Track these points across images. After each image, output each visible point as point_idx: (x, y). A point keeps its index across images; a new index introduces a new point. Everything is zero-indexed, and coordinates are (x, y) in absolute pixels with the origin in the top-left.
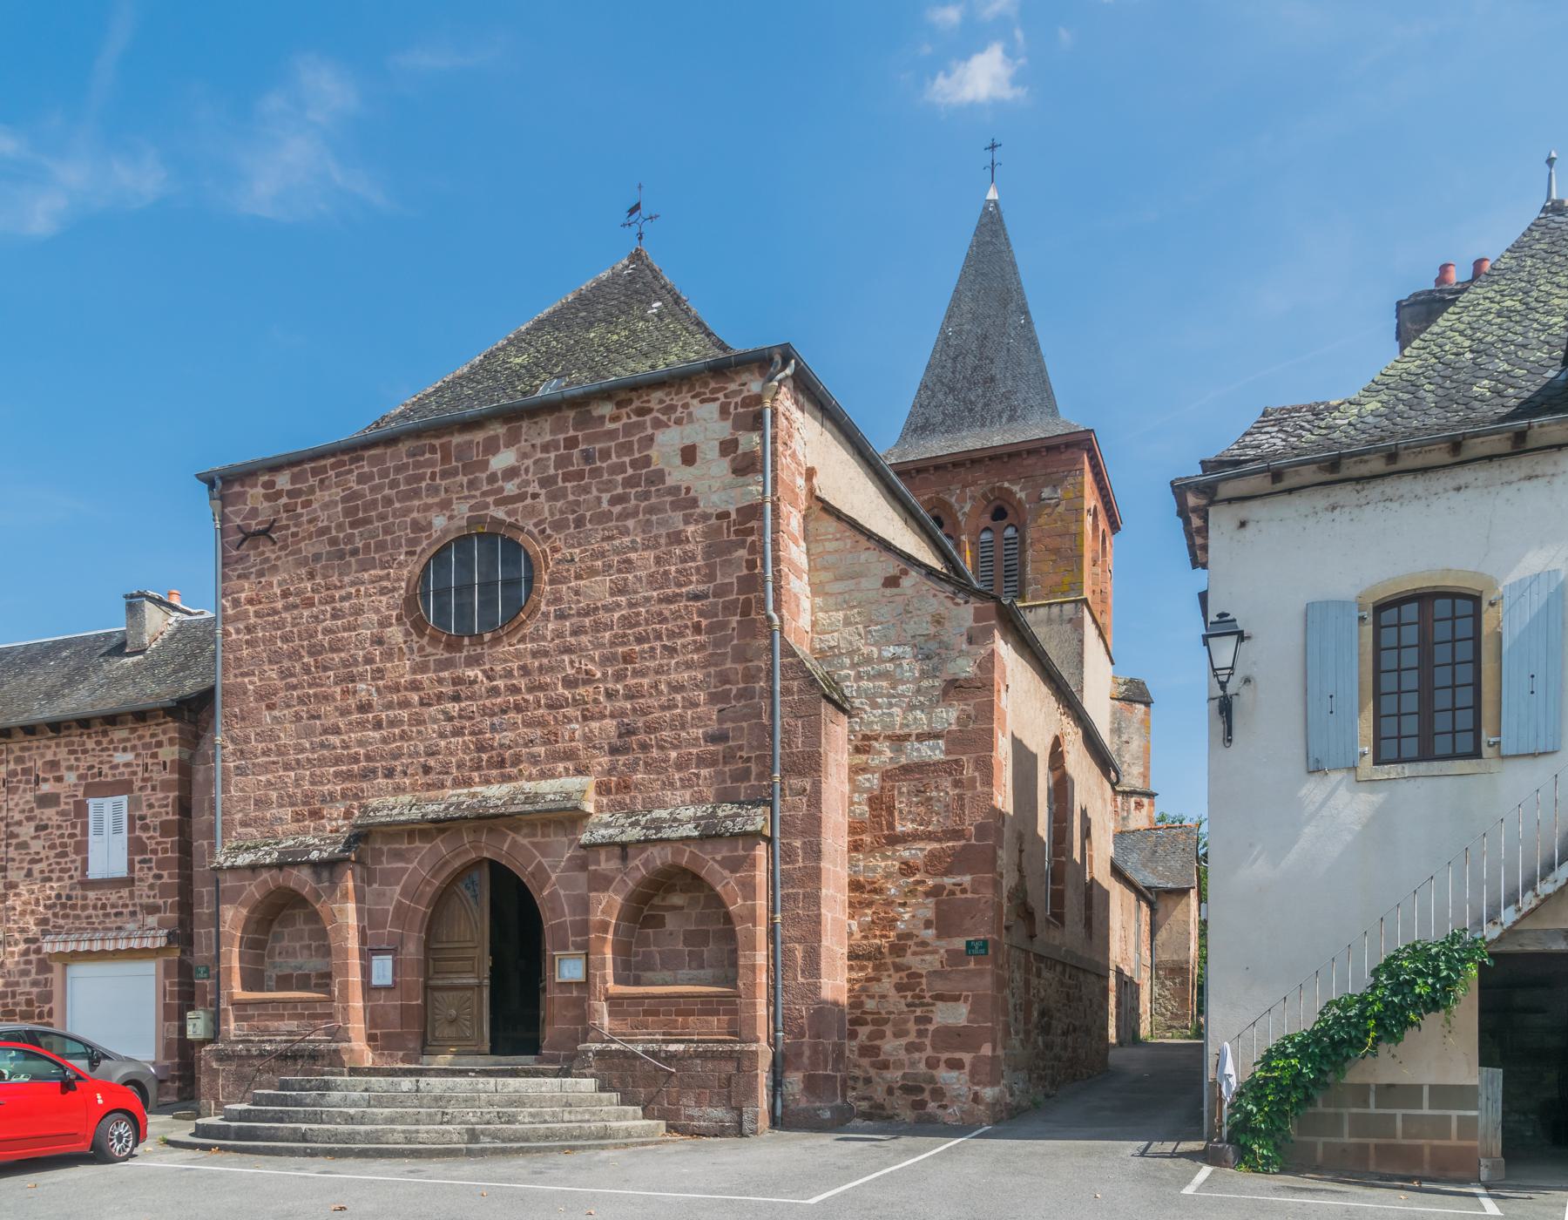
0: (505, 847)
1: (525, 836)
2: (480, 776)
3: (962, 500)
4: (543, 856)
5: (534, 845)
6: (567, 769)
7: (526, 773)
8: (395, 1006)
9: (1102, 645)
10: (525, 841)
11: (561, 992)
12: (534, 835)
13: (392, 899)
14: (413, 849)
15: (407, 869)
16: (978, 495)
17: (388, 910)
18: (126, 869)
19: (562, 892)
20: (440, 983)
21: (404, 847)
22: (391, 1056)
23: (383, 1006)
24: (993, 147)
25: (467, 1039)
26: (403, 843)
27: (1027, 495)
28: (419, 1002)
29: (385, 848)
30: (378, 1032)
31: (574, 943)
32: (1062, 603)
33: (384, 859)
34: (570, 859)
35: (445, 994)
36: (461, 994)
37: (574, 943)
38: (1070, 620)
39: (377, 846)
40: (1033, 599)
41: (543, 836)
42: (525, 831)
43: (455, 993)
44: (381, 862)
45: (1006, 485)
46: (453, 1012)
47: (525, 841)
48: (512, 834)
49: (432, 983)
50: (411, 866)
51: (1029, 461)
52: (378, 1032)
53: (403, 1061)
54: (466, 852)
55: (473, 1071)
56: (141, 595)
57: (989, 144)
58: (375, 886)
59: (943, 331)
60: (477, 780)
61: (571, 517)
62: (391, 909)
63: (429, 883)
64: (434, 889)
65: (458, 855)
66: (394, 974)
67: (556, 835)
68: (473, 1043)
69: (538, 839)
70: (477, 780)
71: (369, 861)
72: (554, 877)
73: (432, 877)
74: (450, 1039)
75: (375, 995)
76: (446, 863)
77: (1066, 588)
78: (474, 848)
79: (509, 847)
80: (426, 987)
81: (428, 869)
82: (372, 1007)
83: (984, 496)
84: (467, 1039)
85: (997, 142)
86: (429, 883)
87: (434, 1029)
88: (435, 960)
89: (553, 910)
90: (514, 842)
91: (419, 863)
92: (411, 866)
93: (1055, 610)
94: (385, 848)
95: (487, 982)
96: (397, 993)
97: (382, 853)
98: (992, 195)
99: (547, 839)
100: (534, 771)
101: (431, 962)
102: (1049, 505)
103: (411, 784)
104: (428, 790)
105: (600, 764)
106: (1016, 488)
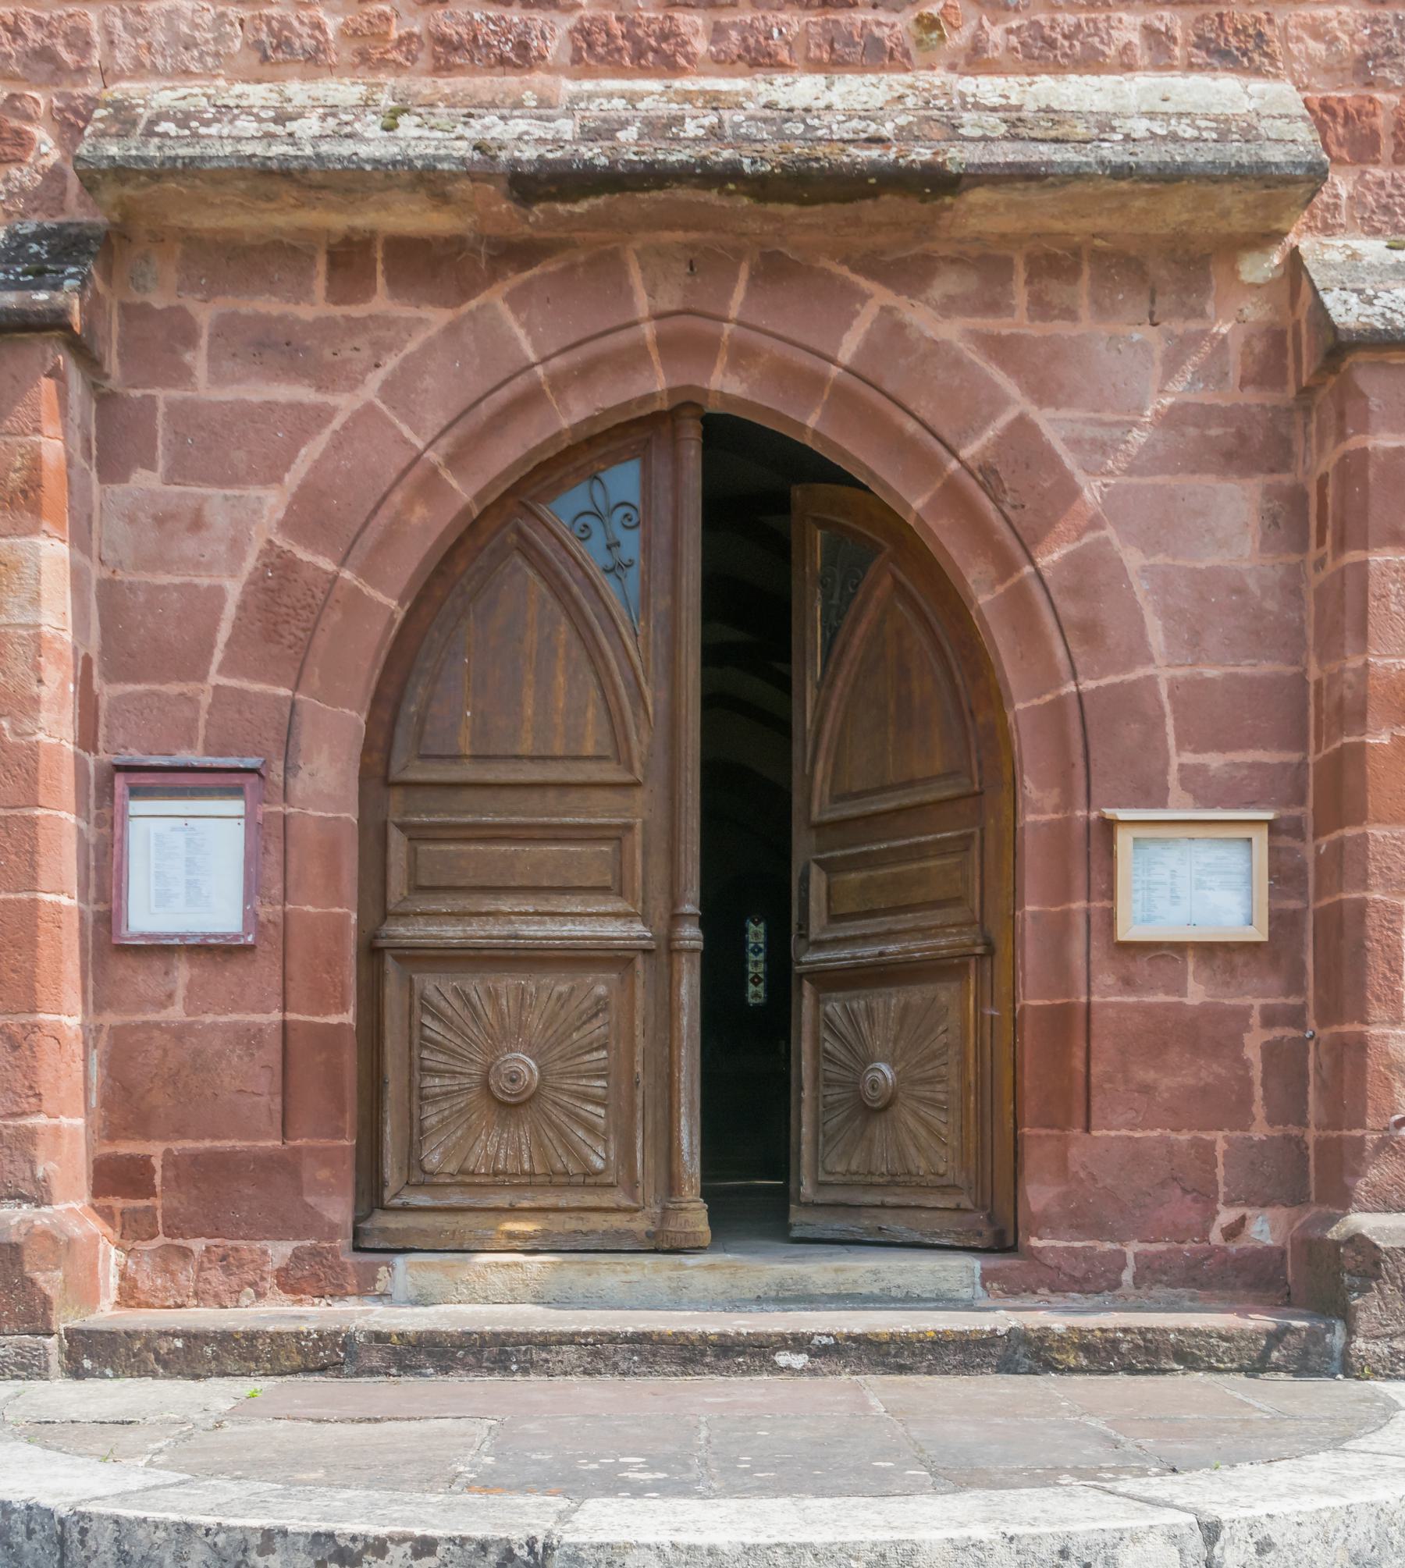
0: (848, 348)
1: (949, 307)
2: (718, 32)
4: (1043, 392)
5: (1000, 348)
6: (1158, 40)
7: (959, 39)
8: (249, 1037)
10: (951, 331)
11: (1128, 983)
12: (995, 306)
13: (237, 546)
14: (355, 326)
15: (321, 415)
17: (218, 593)
19: (1133, 559)
20: (452, 932)
21: (306, 312)
22: (227, 1261)
23: (180, 1033)
25: (590, 1179)
26: (301, 294)
28: (348, 1018)
29: (205, 314)
30: (155, 1150)
31: (1192, 778)
33: (198, 360)
34: (1172, 419)
35: (474, 985)
36: (560, 984)
37: (1192, 778)
39: (158, 300)
41: (1041, 308)
42: (947, 284)
43: (528, 982)
44: (182, 375)
46: (524, 1065)
47: (951, 331)
48: (881, 295)
49: (403, 931)
50: (345, 403)
52: (155, 1150)
53: (291, 1283)
54: (633, 358)
55: (798, 1342)
58: (146, 481)
60: (701, 46)
61: (41, 98)
62: (234, 590)
63: (430, 486)
64: (448, 515)
65: (586, 373)
66: (254, 886)
67: (1103, 310)
68: (618, 1198)
69: (1017, 322)
70: (701, 46)
71: (113, 365)
72: (1091, 491)
73: (453, 460)
74: (498, 1179)
75: (143, 979)
76: (530, 399)
78: (671, 346)
79: (869, 348)
80: (372, 952)
81: (435, 419)
82: (117, 1033)
84: (590, 1179)
86: (430, 486)
87: (415, 1137)
88: (417, 834)
89: (1090, 632)
90: (893, 329)
91: (388, 388)
92: (345, 403)
94: (205, 314)
95: (691, 934)
96: (265, 972)
97: (188, 336)
99: (1060, 328)
100: (996, 34)
101: (397, 841)
103: (350, 33)
104: (442, 68)
105: (1317, 31)
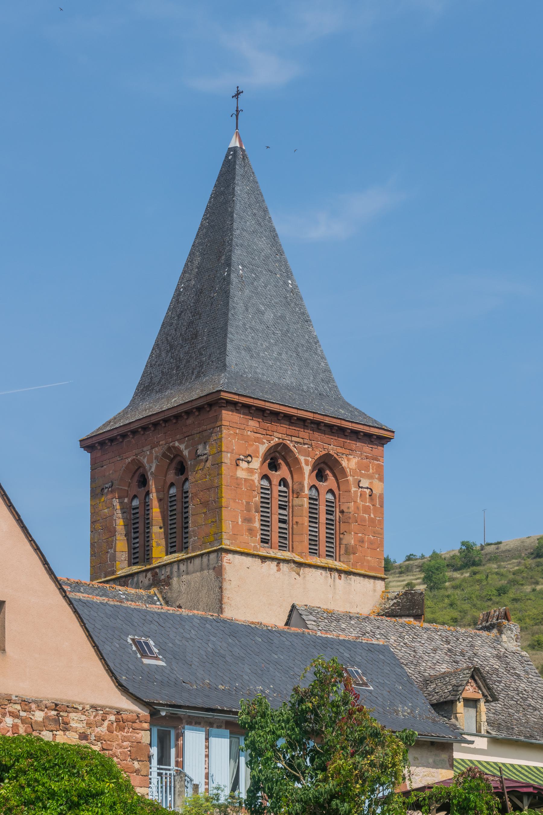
3: (150, 462)
9: (358, 578)
16: (160, 455)
18: (226, 739)
24: (238, 94)
27: (189, 452)
32: (209, 553)
38: (214, 568)
40: (193, 551)
45: (177, 444)
51: (190, 421)
56: (238, 459)
57: (234, 92)
59: (178, 289)
77: (212, 539)
83: (164, 455)
85: (240, 89)
93: (205, 559)
98: (234, 143)
102: (202, 460)
106: (182, 447)
